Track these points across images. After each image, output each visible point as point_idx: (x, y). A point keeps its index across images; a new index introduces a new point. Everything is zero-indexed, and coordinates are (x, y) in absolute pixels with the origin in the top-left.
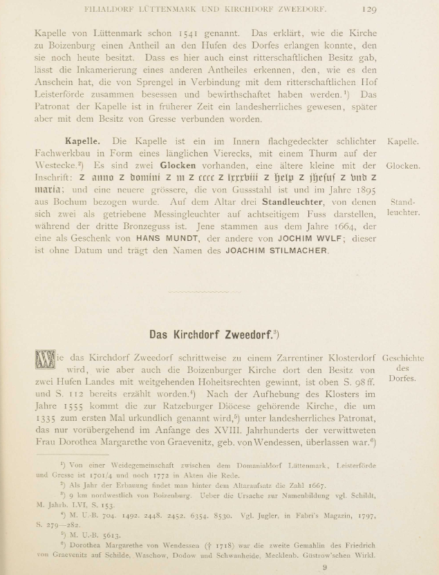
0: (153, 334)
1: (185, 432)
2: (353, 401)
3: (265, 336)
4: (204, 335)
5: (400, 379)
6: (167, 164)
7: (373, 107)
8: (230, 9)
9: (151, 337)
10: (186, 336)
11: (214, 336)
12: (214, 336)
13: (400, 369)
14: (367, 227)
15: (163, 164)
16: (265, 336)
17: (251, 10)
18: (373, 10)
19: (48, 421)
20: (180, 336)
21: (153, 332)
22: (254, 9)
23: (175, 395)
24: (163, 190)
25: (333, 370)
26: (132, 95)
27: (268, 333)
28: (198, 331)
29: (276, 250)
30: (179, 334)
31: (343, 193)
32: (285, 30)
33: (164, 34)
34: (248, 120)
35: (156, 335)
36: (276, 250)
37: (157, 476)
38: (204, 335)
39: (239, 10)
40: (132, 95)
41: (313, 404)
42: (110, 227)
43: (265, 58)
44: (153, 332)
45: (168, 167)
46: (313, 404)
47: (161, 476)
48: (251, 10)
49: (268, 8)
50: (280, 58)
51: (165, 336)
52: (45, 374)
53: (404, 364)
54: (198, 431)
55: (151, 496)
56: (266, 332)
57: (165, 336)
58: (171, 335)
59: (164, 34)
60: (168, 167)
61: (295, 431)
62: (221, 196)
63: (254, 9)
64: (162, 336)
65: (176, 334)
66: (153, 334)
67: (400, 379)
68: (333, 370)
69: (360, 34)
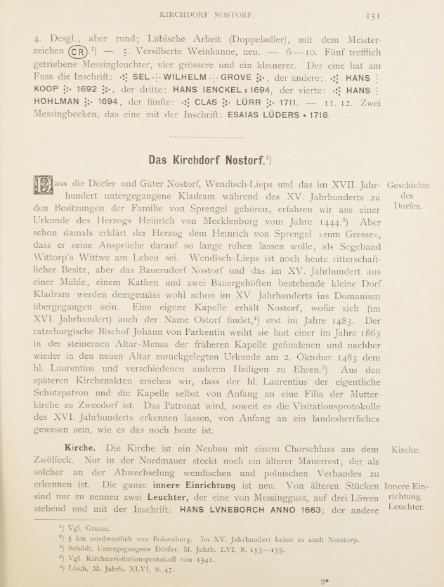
0: (153, 160)
1: (172, 309)
2: (126, 387)
3: (258, 162)
4: (203, 161)
5: (406, 207)
8: (165, 14)
9: (36, 192)
10: (187, 161)
11: (214, 162)
12: (214, 162)
13: (404, 196)
16: (258, 162)
17: (186, 15)
18: (376, 16)
20: (179, 162)
21: (152, 158)
22: (190, 15)
24: (190, 66)
27: (260, 159)
28: (198, 156)
30: (179, 160)
35: (156, 160)
38: (203, 161)
39: (174, 15)
41: (83, 378)
44: (152, 158)
46: (83, 378)
48: (186, 15)
49: (247, 14)
51: (165, 161)
52: (43, 200)
53: (409, 191)
54: (81, 357)
56: (258, 157)
57: (165, 161)
58: (170, 160)
61: (129, 418)
63: (190, 15)
64: (161, 161)
65: (175, 160)
66: (153, 160)
67: (406, 207)
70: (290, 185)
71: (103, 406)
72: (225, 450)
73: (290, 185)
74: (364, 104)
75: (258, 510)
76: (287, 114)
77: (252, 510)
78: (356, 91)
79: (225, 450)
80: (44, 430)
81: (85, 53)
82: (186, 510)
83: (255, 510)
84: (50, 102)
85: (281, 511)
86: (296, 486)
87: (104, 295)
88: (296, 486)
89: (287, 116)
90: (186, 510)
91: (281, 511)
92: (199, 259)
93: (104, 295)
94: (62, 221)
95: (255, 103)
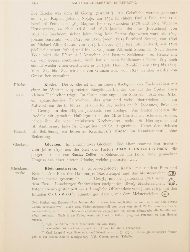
6: (48, 144)
7: (176, 131)
14: (173, 149)
15: (46, 144)
19: (175, 66)
23: (154, 13)
25: (148, 120)
26: (87, 90)
29: (155, 149)
31: (172, 145)
32: (162, 83)
33: (57, 50)
34: (154, 13)
36: (155, 149)
37: (126, 233)
40: (87, 90)
42: (117, 116)
43: (161, 178)
45: (48, 145)
47: (128, 233)
50: (59, 101)
55: (132, 194)
59: (57, 50)
60: (48, 145)
62: (127, 176)
68: (148, 120)
69: (49, 85)
70: (93, 144)
71: (132, 85)
72: (158, 70)
73: (93, 144)
74: (107, 155)
75: (165, 149)
76: (134, 149)
77: (147, 149)
78: (144, 149)
79: (158, 70)
80: (138, 34)
81: (174, 174)
82: (142, 149)
83: (163, 149)
84: (141, 148)
85: (139, 150)
86: (36, 71)
87: (88, 66)
88: (36, 71)
89: (134, 149)
90: (142, 149)
91: (139, 150)
92: (54, 90)
93: (88, 66)
94: (108, 106)
95: (137, 149)
